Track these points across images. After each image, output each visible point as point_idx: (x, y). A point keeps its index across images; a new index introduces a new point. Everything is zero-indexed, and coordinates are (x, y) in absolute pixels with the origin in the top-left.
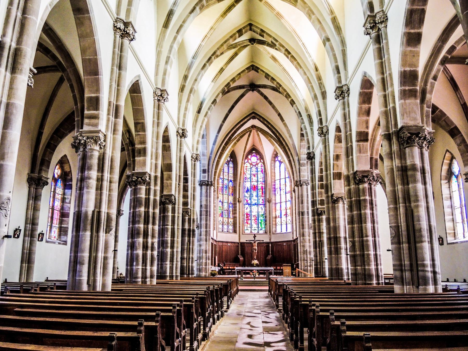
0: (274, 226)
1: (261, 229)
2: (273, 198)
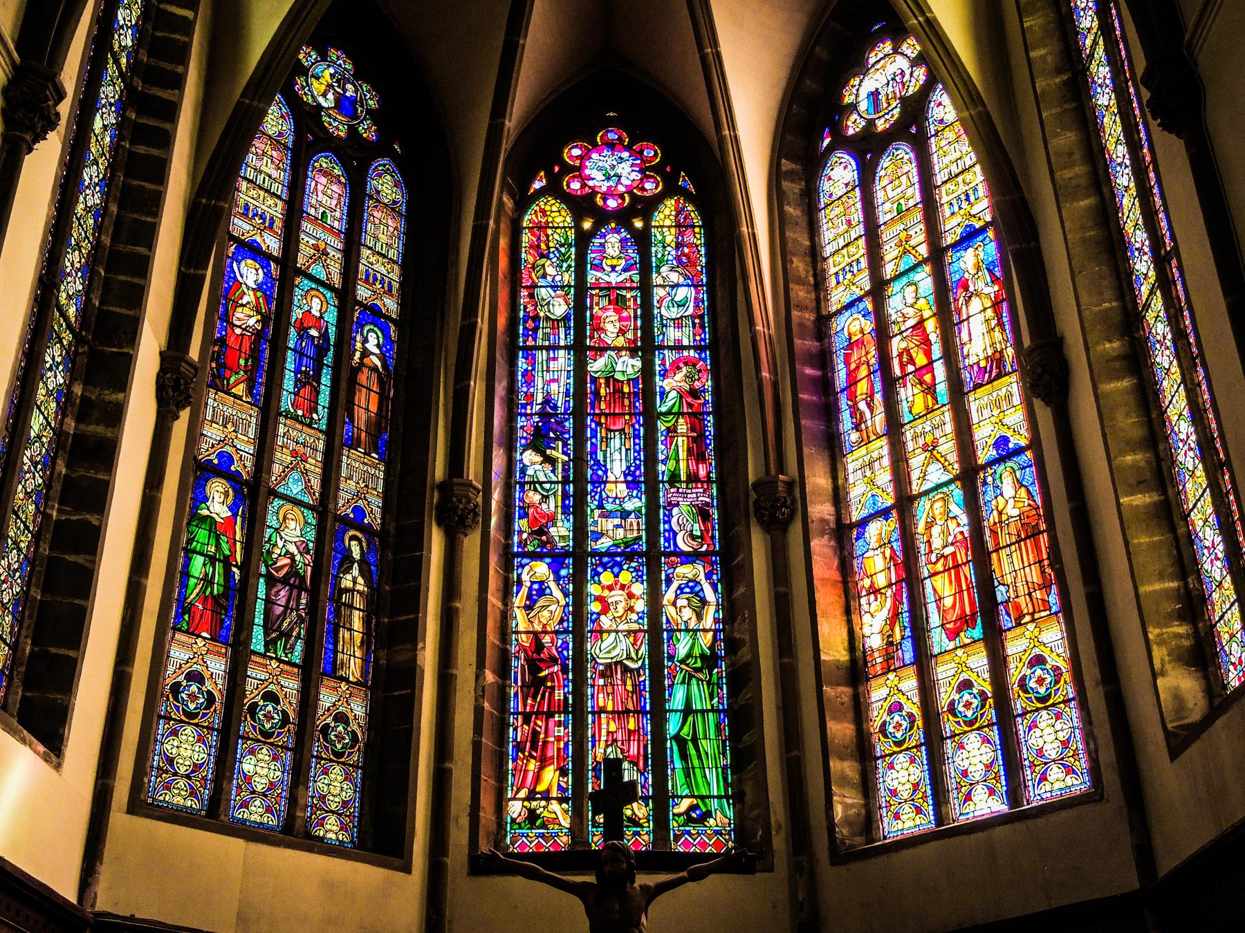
0: (844, 768)
1: (559, 739)
2: (818, 479)
